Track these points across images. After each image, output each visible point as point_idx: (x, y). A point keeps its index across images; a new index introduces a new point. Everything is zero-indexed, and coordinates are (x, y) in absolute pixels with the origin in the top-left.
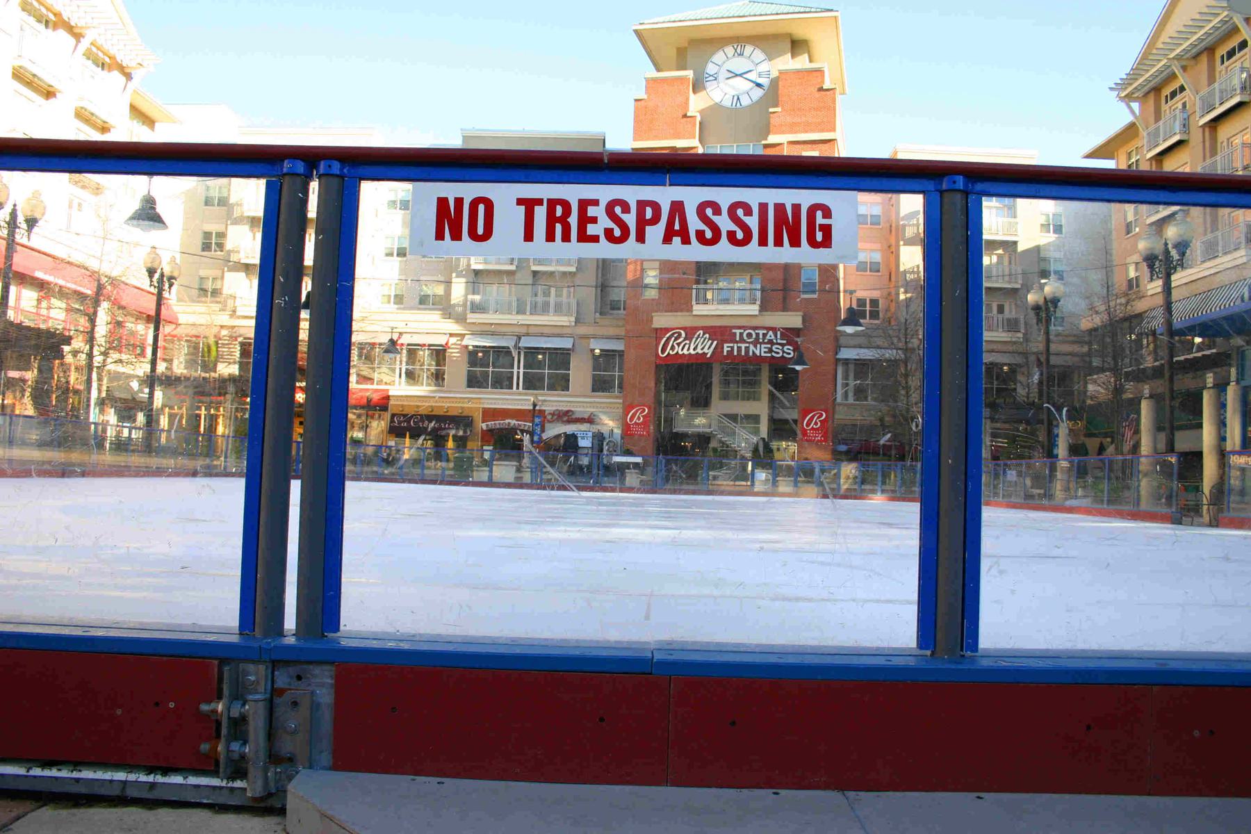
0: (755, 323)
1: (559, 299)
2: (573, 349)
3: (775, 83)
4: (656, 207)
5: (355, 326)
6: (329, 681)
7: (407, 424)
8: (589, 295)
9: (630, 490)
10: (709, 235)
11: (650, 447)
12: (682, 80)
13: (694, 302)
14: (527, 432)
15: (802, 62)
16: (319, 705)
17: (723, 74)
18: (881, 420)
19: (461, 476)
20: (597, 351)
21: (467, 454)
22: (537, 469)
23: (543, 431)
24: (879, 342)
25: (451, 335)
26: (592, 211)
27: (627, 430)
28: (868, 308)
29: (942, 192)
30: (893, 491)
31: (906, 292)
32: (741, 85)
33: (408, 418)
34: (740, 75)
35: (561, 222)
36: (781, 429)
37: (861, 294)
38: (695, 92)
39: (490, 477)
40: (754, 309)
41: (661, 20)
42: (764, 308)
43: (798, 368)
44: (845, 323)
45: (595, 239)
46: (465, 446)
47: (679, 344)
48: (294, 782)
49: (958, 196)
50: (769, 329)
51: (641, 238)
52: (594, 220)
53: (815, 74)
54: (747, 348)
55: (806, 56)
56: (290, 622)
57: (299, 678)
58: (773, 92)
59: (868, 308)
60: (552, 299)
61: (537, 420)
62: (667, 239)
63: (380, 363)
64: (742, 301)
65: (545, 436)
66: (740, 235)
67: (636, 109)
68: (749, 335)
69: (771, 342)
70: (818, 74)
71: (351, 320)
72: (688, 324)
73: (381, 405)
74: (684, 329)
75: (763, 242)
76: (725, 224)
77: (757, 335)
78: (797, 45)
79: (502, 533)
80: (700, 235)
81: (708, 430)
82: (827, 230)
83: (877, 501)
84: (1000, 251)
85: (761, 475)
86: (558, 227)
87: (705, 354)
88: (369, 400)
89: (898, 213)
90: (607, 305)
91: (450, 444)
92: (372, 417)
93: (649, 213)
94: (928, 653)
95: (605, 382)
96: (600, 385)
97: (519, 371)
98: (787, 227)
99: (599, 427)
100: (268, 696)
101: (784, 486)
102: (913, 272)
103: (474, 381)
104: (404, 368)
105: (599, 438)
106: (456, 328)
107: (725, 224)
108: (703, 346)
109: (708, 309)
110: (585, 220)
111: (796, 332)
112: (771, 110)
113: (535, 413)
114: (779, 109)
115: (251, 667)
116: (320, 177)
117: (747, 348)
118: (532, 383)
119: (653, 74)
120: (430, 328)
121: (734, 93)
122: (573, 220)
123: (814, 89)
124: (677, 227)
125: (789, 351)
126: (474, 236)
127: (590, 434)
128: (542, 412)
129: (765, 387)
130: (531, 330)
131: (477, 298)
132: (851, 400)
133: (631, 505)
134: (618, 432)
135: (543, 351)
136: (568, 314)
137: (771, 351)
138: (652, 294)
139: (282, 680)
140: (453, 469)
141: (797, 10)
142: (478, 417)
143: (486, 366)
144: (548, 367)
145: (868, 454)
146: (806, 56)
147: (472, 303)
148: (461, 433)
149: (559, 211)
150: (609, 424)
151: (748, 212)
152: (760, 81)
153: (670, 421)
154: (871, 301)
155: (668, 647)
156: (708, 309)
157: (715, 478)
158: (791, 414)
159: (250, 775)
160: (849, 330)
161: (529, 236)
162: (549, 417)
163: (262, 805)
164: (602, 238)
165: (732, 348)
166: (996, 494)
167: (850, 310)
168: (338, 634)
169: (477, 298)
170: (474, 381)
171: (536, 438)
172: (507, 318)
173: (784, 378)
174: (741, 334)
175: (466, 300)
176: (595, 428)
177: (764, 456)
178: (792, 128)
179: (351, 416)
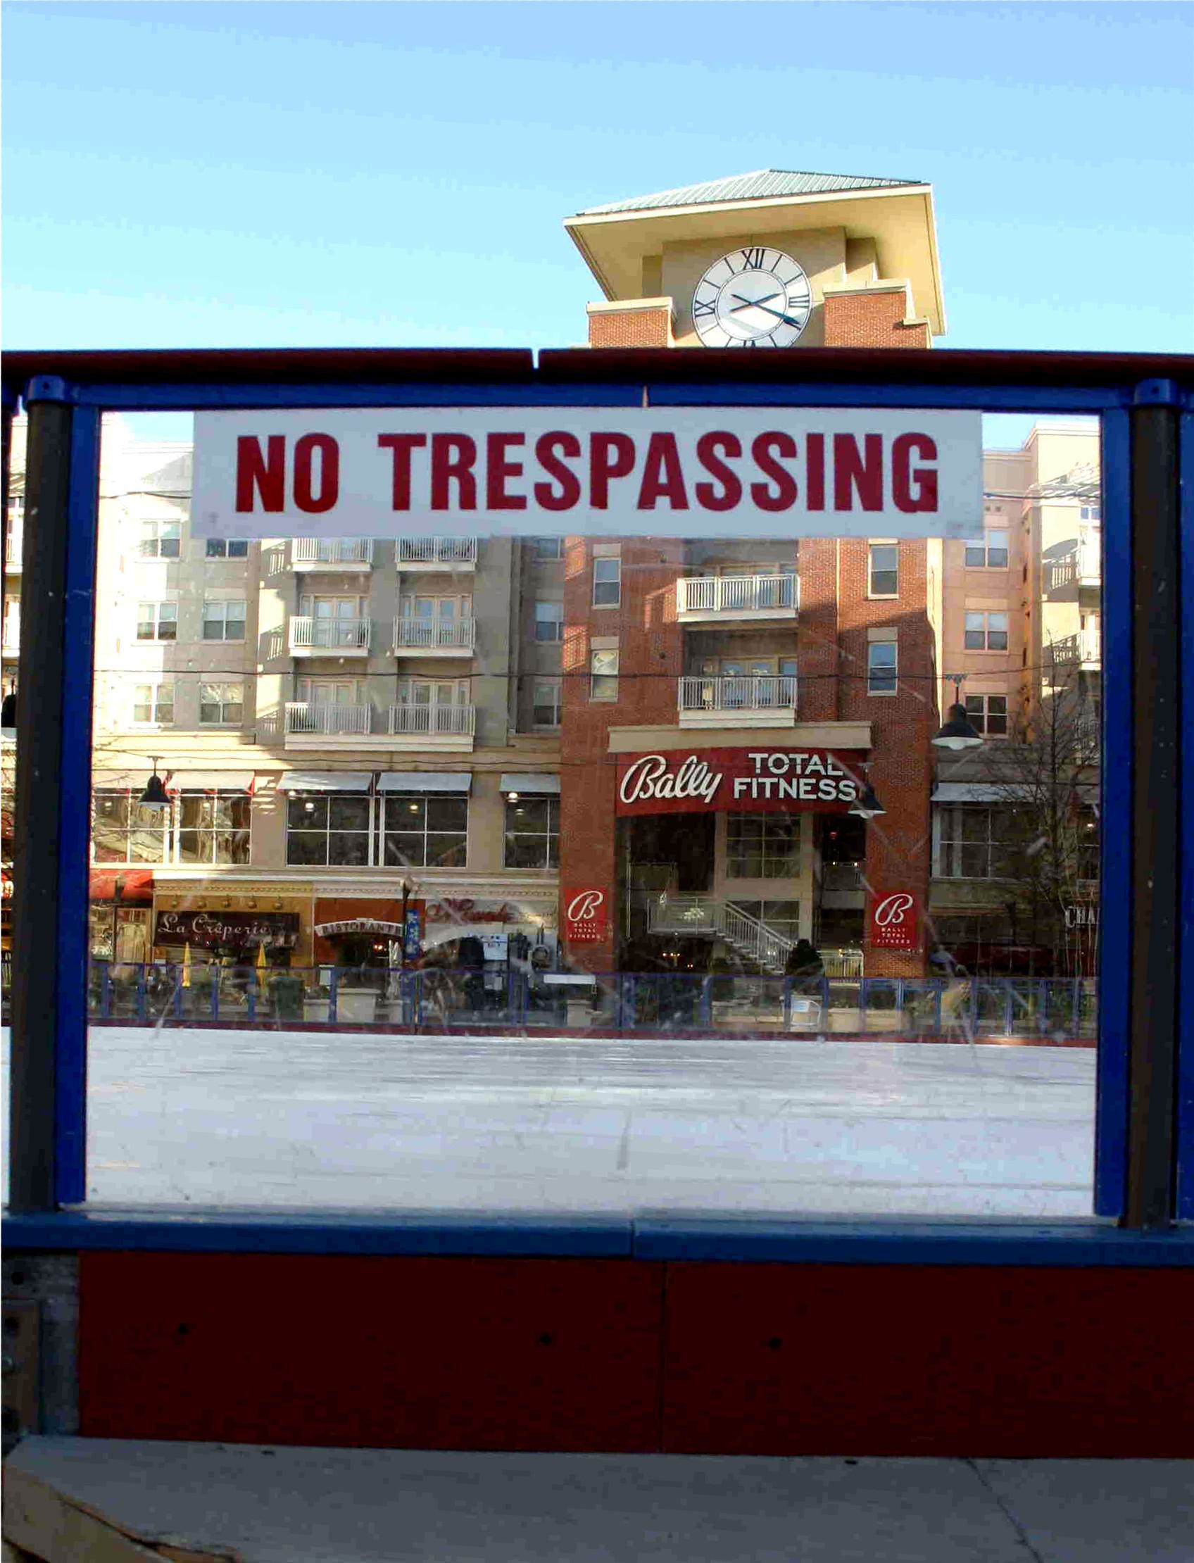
0: (789, 742)
1: (445, 706)
2: (470, 793)
5: (96, 757)
6: (72, 1283)
7: (182, 925)
8: (495, 693)
9: (573, 1033)
12: (656, 311)
13: (680, 707)
15: (865, 278)
16: (52, 1324)
17: (725, 304)
18: (1011, 907)
19: (284, 1011)
20: (513, 796)
23: (422, 935)
24: (1007, 771)
25: (258, 773)
26: (512, 454)
27: (563, 924)
28: (986, 713)
29: (1132, 411)
34: (757, 304)
36: (838, 925)
37: (971, 687)
39: (333, 1015)
40: (786, 717)
42: (800, 716)
44: (950, 731)
45: (518, 503)
46: (286, 964)
47: (655, 781)
49: (1162, 416)
50: (811, 751)
51: (599, 500)
52: (516, 470)
53: (889, 299)
54: (775, 787)
55: (872, 267)
59: (986, 713)
60: (433, 707)
61: (411, 917)
62: (646, 501)
63: (135, 824)
64: (765, 703)
65: (425, 946)
66: (774, 491)
68: (779, 763)
69: (815, 774)
71: (88, 749)
72: (668, 746)
73: (139, 898)
75: (816, 502)
76: (747, 470)
77: (793, 761)
78: (857, 248)
79: (359, 1097)
80: (704, 493)
81: (707, 930)
82: (929, 481)
86: (454, 484)
87: (701, 797)
88: (119, 889)
89: (1038, 543)
90: (530, 716)
91: (261, 960)
92: (126, 919)
94: (1113, 1221)
96: (521, 855)
97: (377, 831)
98: (858, 476)
99: (521, 927)
102: (1065, 649)
103: (301, 852)
105: (519, 944)
106: (259, 758)
107: (747, 470)
108: (698, 784)
109: (710, 717)
110: (500, 470)
111: (862, 754)
113: (407, 908)
116: (28, 407)
117: (775, 787)
118: (403, 850)
120: (217, 761)
122: (480, 470)
124: (663, 479)
125: (850, 790)
127: (504, 938)
128: (418, 906)
129: (807, 855)
131: (302, 706)
132: (957, 874)
133: (580, 1054)
134: (551, 936)
137: (815, 789)
138: (608, 693)
142: (309, 916)
143: (321, 827)
144: (429, 825)
146: (872, 267)
148: (281, 941)
149: (454, 455)
150: (534, 921)
152: (792, 313)
153: (641, 915)
154: (992, 700)
156: (710, 717)
157: (723, 1012)
160: (955, 743)
161: (402, 501)
162: (432, 913)
165: (749, 785)
167: (956, 710)
168: (82, 1206)
169: (302, 706)
171: (410, 949)
173: (840, 836)
174: (764, 761)
175: (283, 710)
176: (511, 929)
177: (803, 964)
179: (93, 919)
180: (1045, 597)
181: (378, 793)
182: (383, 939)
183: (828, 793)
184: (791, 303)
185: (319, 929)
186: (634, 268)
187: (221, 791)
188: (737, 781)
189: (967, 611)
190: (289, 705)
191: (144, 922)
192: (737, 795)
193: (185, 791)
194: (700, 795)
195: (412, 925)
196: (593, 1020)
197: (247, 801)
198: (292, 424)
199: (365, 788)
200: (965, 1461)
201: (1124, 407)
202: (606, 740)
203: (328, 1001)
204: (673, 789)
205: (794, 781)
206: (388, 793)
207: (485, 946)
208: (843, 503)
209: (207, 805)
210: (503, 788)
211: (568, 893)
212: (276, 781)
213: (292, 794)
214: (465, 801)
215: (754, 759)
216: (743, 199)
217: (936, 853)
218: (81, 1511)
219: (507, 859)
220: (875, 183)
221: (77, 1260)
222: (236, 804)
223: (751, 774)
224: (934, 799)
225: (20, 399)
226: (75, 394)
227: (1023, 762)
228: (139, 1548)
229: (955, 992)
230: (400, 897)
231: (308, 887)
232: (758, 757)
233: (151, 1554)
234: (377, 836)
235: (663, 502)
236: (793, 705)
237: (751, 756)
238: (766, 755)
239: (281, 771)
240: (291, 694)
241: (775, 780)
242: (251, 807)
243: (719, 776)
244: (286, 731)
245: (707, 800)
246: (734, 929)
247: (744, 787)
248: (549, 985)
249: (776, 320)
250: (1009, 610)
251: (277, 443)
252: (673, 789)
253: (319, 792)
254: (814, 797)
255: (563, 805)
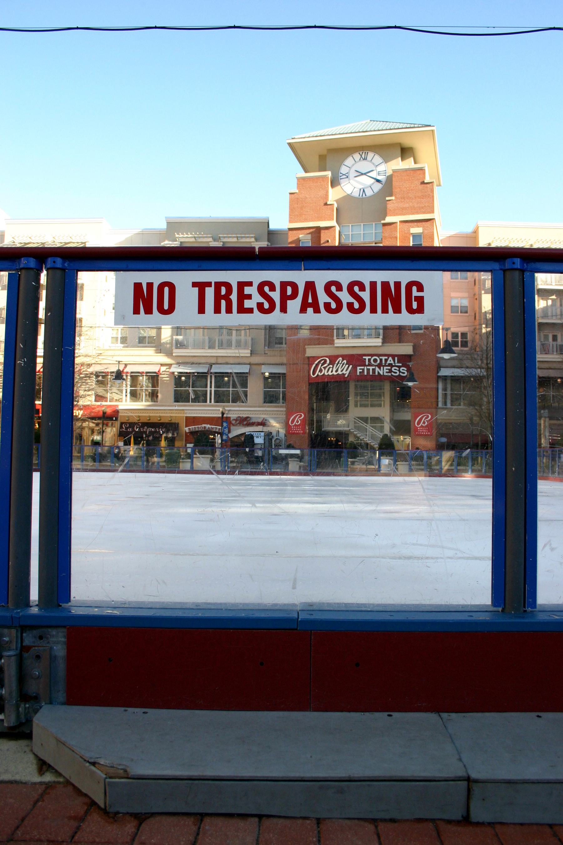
3: (390, 179)
4: (294, 286)
6: (63, 639)
9: (293, 474)
10: (333, 306)
11: (306, 441)
12: (324, 178)
13: (335, 338)
14: (218, 433)
15: (409, 164)
17: (352, 174)
18: (471, 419)
19: (172, 465)
21: (175, 450)
22: (224, 461)
25: (162, 365)
26: (247, 290)
27: (287, 427)
28: (460, 339)
29: (504, 271)
30: (480, 471)
31: (487, 327)
32: (366, 181)
33: (132, 425)
34: (365, 174)
35: (225, 299)
37: (453, 330)
38: (332, 186)
40: (378, 342)
41: (307, 135)
42: (384, 341)
43: (410, 384)
44: (444, 351)
45: (250, 311)
47: (325, 368)
48: (38, 715)
49: (517, 273)
50: (388, 356)
51: (284, 309)
52: (249, 297)
53: (419, 172)
54: (374, 370)
55: (412, 159)
56: (34, 595)
57: (41, 638)
58: (388, 186)
59: (460, 339)
61: (225, 424)
62: (303, 310)
63: (111, 386)
64: (369, 336)
66: (356, 306)
67: (291, 201)
68: (375, 361)
69: (390, 365)
70: (421, 172)
74: (329, 357)
75: (373, 310)
76: (345, 297)
77: (381, 360)
78: (405, 152)
81: (347, 429)
82: (420, 300)
83: (468, 478)
84: (554, 297)
85: (386, 461)
86: (223, 303)
87: (344, 374)
88: (104, 413)
91: (163, 443)
92: (107, 425)
93: (289, 291)
95: (272, 396)
97: (211, 389)
98: (391, 298)
100: (18, 652)
101: (403, 466)
103: (180, 397)
104: (129, 389)
107: (345, 297)
108: (343, 369)
110: (242, 297)
112: (387, 199)
113: (223, 420)
114: (393, 198)
115: (6, 631)
116: (47, 270)
117: (374, 370)
118: (220, 398)
119: (303, 174)
120: (146, 360)
121: (361, 187)
122: (234, 297)
123: (418, 183)
124: (310, 300)
125: (404, 372)
126: (161, 310)
127: (262, 434)
129: (387, 399)
130: (220, 361)
131: (180, 338)
132: (449, 405)
133: (293, 485)
134: (282, 432)
135: (228, 374)
136: (245, 348)
137: (390, 371)
139: (28, 639)
140: (165, 461)
141: (405, 126)
142: (183, 424)
143: (187, 387)
144: (229, 386)
145: (459, 447)
146: (412, 159)
147: (177, 341)
149: (223, 291)
150: (276, 426)
151: (362, 288)
152: (379, 178)
154: (462, 334)
155: (310, 608)
157: (353, 463)
158: (406, 416)
159: (6, 710)
160: (446, 356)
161: (202, 310)
163: (17, 731)
164: (256, 310)
165: (363, 370)
166: (553, 472)
167: (446, 342)
168: (70, 604)
169: (180, 338)
170: (180, 397)
172: (203, 354)
174: (369, 360)
175: (172, 339)
176: (266, 429)
177: (387, 447)
178: (403, 211)
180: (483, 292)
181: (211, 373)
182: (214, 433)
183: (396, 373)
184: (379, 174)
185: (187, 429)
186: (316, 160)
187: (147, 373)
188: (358, 368)
189: (451, 298)
190: (174, 337)
191: (115, 427)
192: (358, 374)
193: (132, 373)
194: (343, 374)
195: (225, 428)
196: (300, 467)
197: (158, 376)
198: (156, 278)
199: (206, 371)
200: (437, 714)
201: (501, 269)
202: (304, 351)
203: (190, 460)
204: (332, 371)
205: (382, 368)
206: (216, 373)
207: (255, 438)
208: (385, 310)
209: (141, 378)
210: (263, 371)
211: (289, 414)
212: (170, 368)
213: (176, 373)
214: (247, 377)
215: (365, 359)
216: (359, 132)
217: (440, 399)
218: (64, 744)
219: (292, 209)
220: (412, 126)
221: (65, 630)
222: (153, 377)
223: (365, 365)
224: (439, 374)
225: (44, 266)
226: (66, 265)
227: (473, 359)
228: (88, 764)
229: (447, 455)
230: (221, 416)
231: (182, 412)
232: (367, 358)
233: (93, 768)
234: (211, 391)
235: (310, 310)
236: (381, 337)
237: (364, 357)
238: (370, 357)
239: (171, 365)
240: (175, 334)
241: (374, 367)
242: (159, 379)
243: (351, 366)
244: (174, 348)
245: (346, 376)
246: (358, 428)
247: (361, 371)
248: (281, 454)
249: (373, 181)
250: (468, 297)
251: (150, 286)
252: (332, 371)
253: (187, 373)
254: (390, 374)
255: (287, 378)
